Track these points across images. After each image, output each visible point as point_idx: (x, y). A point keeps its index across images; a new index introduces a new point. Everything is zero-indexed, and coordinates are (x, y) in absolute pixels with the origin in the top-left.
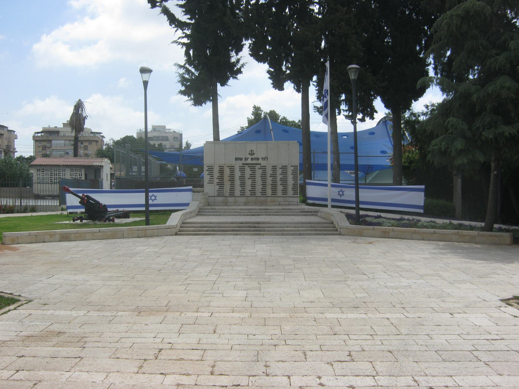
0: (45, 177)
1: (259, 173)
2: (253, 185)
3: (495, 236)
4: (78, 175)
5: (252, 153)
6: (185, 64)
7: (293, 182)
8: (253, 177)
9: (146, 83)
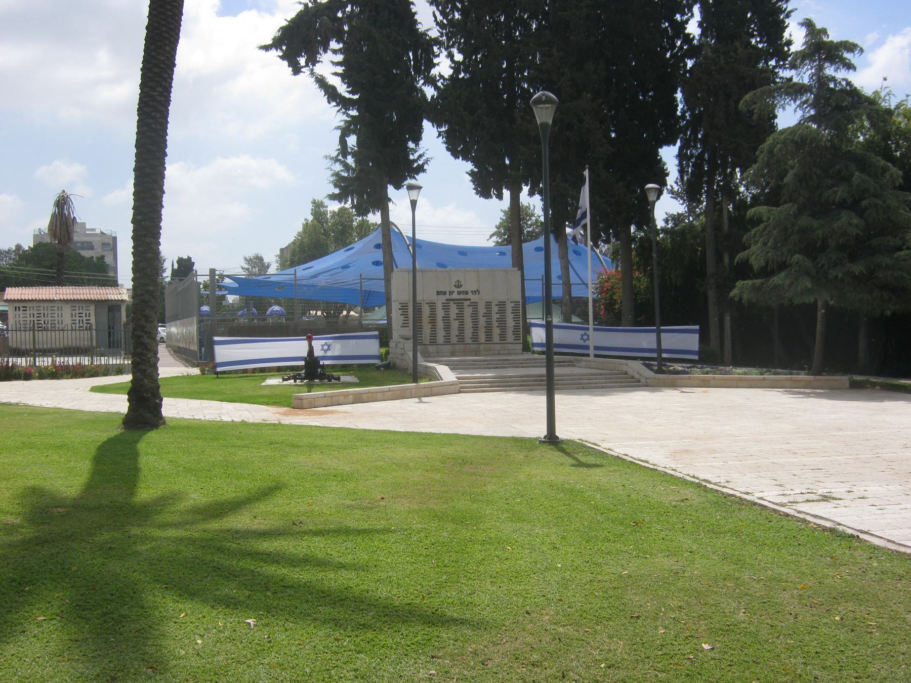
0: (28, 319)
1: (468, 311)
2: (461, 329)
3: (820, 380)
4: (84, 315)
5: (458, 285)
6: (338, 155)
7: (513, 324)
8: (460, 317)
9: (414, 204)
